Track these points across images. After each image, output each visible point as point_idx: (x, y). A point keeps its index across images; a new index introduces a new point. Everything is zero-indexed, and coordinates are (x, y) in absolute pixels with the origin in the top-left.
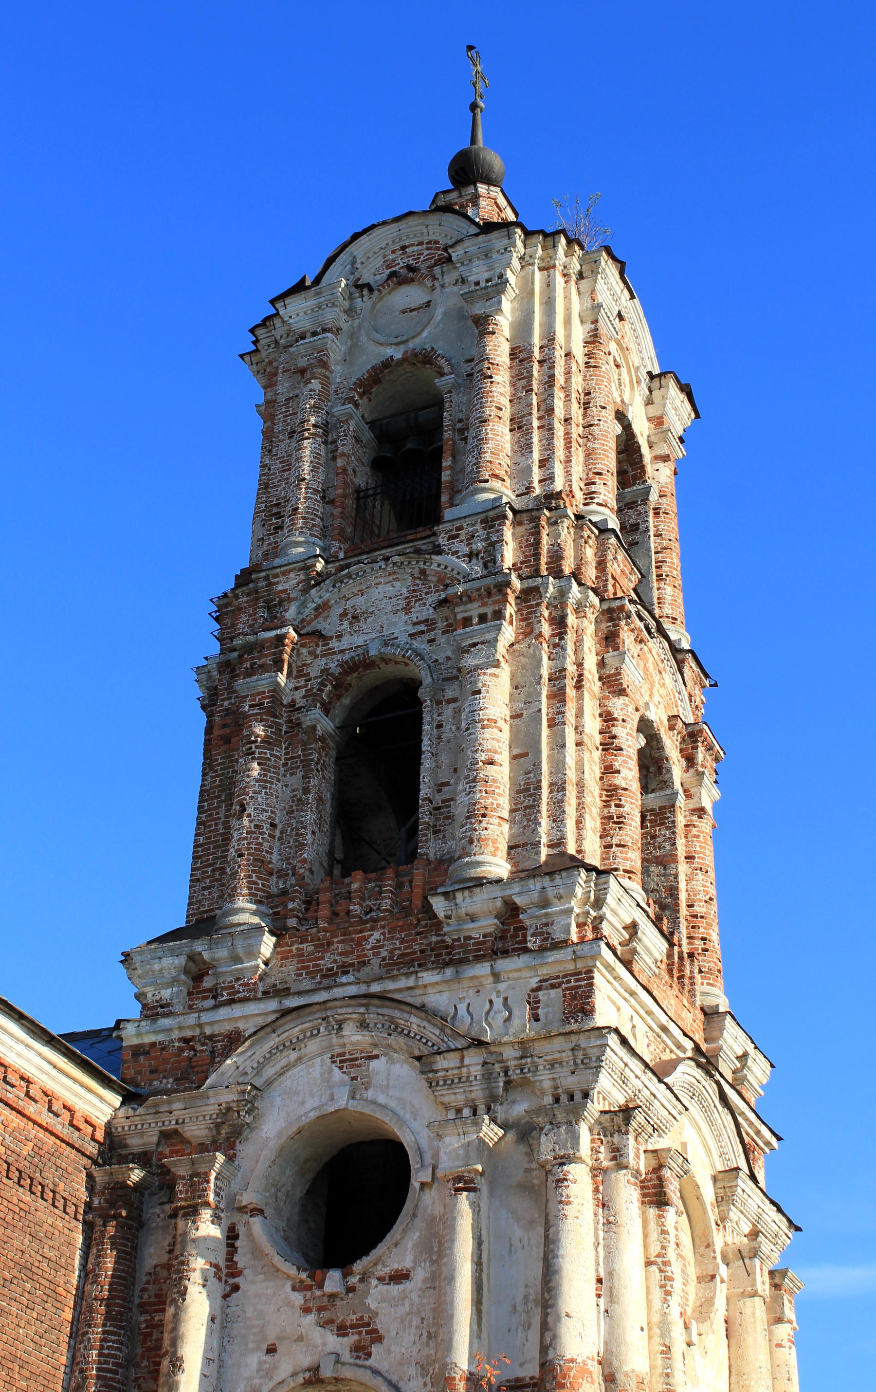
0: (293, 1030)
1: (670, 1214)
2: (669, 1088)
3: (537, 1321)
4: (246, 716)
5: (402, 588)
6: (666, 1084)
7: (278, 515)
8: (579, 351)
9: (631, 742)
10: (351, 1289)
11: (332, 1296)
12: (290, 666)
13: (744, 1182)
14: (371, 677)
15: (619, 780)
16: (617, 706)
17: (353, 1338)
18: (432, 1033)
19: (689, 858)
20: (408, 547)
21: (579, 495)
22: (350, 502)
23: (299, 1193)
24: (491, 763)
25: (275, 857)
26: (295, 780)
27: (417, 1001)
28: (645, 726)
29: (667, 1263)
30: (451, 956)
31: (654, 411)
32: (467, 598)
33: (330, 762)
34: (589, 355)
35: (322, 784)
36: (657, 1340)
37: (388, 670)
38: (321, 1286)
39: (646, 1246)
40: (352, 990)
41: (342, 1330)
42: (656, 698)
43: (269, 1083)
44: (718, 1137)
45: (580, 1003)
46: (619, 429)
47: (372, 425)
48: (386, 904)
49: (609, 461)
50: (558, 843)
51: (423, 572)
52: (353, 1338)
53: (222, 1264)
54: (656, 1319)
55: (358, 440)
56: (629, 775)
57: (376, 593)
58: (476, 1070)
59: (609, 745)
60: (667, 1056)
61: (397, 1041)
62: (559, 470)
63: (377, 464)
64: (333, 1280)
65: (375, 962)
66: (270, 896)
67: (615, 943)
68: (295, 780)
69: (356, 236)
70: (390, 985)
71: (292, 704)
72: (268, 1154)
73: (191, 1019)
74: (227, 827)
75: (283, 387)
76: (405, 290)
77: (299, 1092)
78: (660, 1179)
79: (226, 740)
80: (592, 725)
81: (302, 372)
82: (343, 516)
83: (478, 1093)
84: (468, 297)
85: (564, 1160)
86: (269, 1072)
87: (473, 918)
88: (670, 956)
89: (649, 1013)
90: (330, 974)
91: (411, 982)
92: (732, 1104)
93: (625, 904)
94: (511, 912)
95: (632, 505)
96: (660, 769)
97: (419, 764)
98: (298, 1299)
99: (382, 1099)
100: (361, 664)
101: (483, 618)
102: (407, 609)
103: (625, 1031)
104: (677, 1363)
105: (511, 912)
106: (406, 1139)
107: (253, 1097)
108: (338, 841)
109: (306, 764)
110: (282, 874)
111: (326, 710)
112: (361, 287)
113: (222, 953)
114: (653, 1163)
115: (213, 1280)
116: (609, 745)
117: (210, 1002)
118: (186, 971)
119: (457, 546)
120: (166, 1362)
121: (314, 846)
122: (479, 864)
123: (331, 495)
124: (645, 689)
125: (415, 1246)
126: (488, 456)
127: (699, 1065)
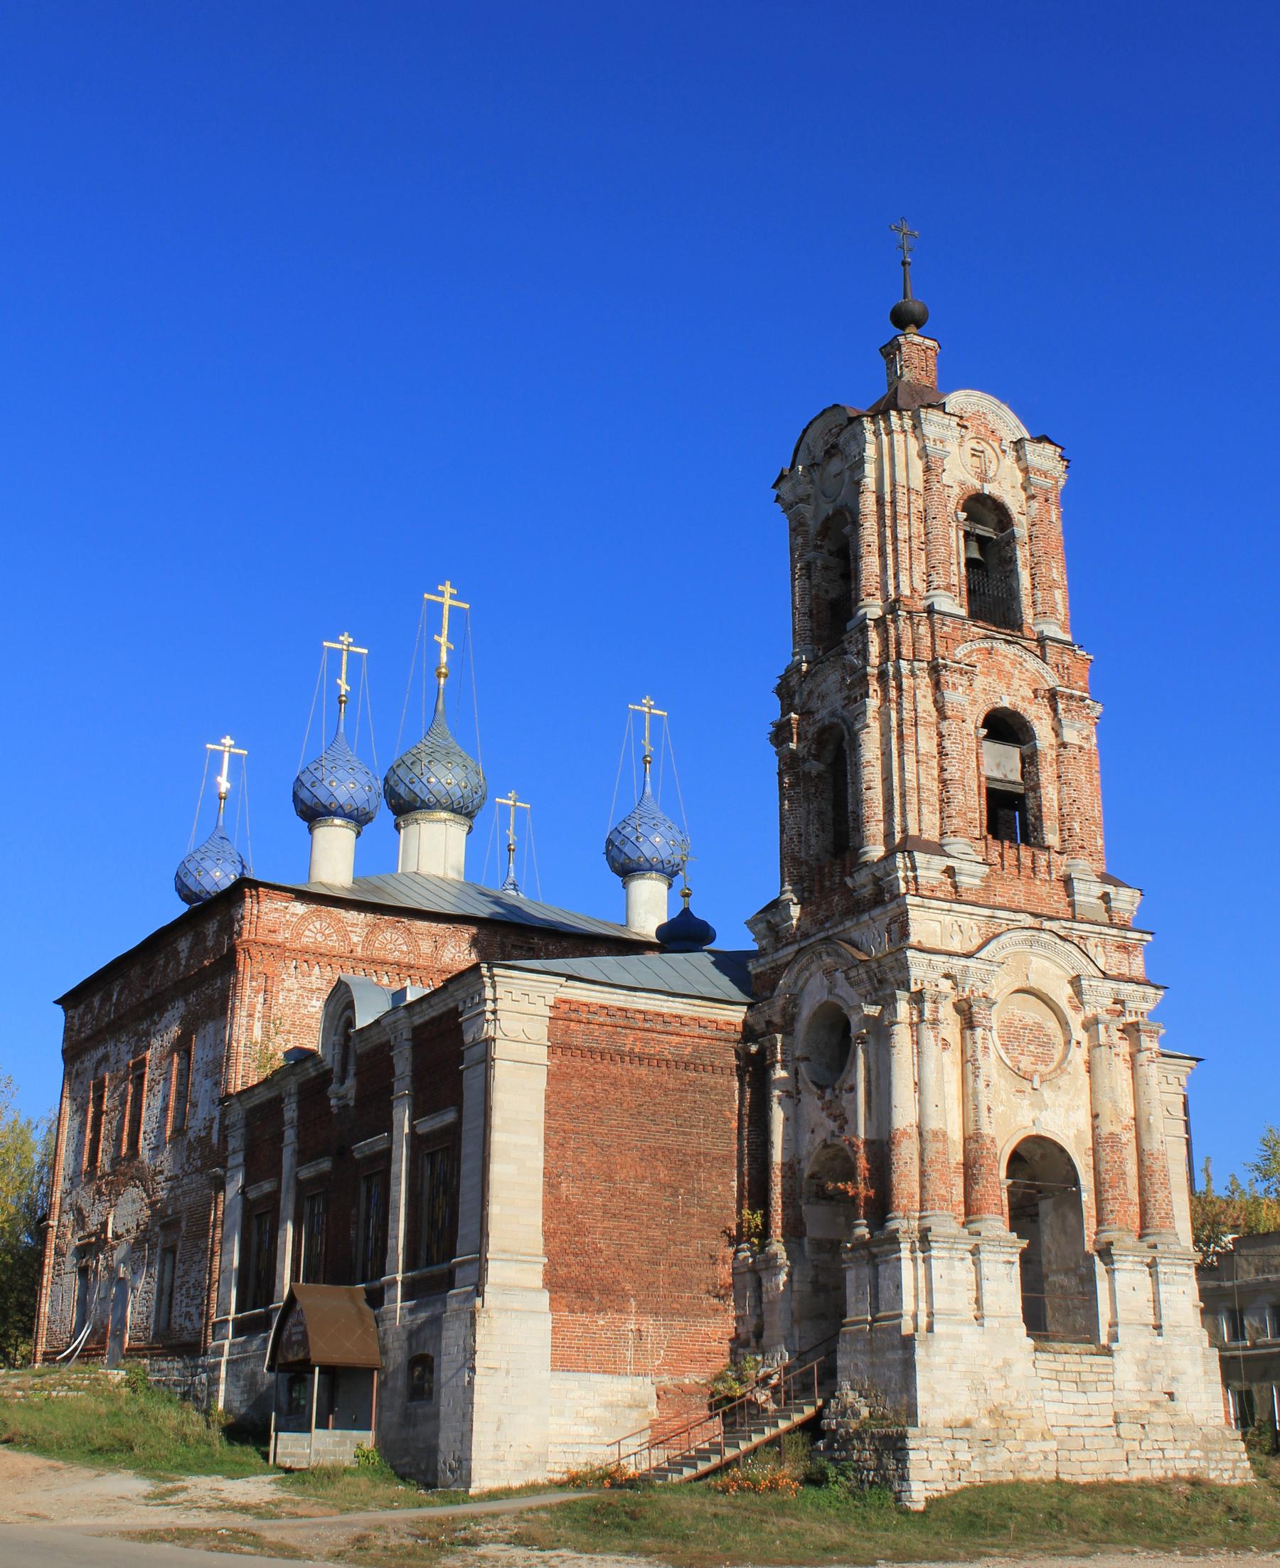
12: (798, 734)
24: (869, 788)
25: (803, 854)
43: (802, 989)
50: (904, 830)
58: (864, 976)
69: (805, 431)
85: (893, 1024)
86: (800, 983)
92: (391, 1198)
107: (794, 1000)
115: (784, 1099)
122: (865, 853)
126: (863, 583)
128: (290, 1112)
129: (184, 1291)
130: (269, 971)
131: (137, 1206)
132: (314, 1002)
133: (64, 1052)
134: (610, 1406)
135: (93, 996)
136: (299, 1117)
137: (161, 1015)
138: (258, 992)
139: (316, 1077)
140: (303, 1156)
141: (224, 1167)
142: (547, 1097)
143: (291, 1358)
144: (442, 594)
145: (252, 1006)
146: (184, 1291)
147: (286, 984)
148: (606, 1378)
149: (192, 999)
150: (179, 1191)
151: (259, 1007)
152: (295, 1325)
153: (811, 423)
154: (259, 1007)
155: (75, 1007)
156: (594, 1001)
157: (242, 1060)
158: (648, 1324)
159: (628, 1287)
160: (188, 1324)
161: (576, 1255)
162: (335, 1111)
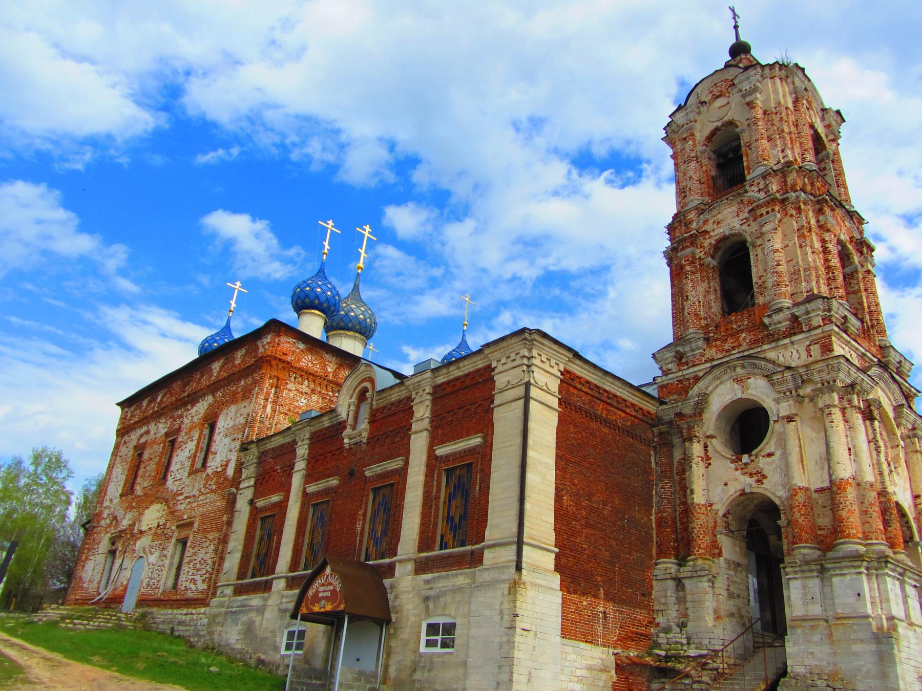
0: (717, 372)
1: (876, 423)
2: (869, 376)
3: (826, 466)
4: (684, 265)
5: (735, 208)
6: (869, 376)
7: (684, 192)
8: (790, 106)
9: (833, 248)
10: (752, 461)
11: (746, 464)
13: (906, 410)
14: (728, 243)
15: (832, 264)
16: (827, 236)
17: (755, 478)
18: (770, 366)
19: (866, 290)
20: (735, 193)
21: (799, 160)
22: (711, 182)
23: (728, 429)
25: (702, 313)
26: (705, 285)
27: (763, 356)
28: (839, 242)
29: (877, 441)
30: (773, 337)
31: (826, 123)
32: (761, 206)
33: (717, 275)
34: (795, 106)
35: (716, 284)
36: (876, 470)
37: (734, 239)
38: (741, 460)
39: (867, 435)
40: (738, 355)
41: (751, 475)
42: (843, 231)
44: (893, 394)
45: (827, 348)
46: (812, 132)
47: (714, 152)
48: (746, 323)
49: (810, 144)
51: (742, 201)
52: (755, 478)
53: (703, 455)
54: (875, 462)
55: (710, 159)
56: (835, 261)
57: (725, 212)
58: (789, 378)
59: (825, 251)
60: (867, 365)
61: (756, 371)
62: (789, 152)
63: (719, 166)
64: (745, 458)
65: (745, 344)
66: (702, 327)
67: (839, 324)
68: (705, 285)
70: (752, 352)
71: (700, 258)
72: (714, 417)
73: (680, 373)
74: (683, 305)
75: (679, 146)
76: (719, 100)
77: (722, 395)
78: (871, 410)
79: (678, 275)
80: (817, 245)
81: (685, 139)
82: (708, 187)
83: (791, 386)
84: (744, 96)
86: (710, 388)
87: (780, 323)
88: (863, 327)
89: (857, 349)
90: (728, 351)
91: (759, 349)
93: (840, 308)
94: (795, 319)
95: (822, 161)
96: (849, 258)
97: (751, 271)
98: (733, 466)
99: (754, 393)
100: (724, 239)
101: (767, 213)
102: (738, 216)
103: (848, 356)
104: (887, 478)
105: (795, 319)
106: (765, 406)
108: (725, 305)
109: (708, 278)
110: (705, 319)
111: (713, 257)
112: (703, 103)
113: (687, 349)
114: (866, 404)
116: (825, 251)
117: (686, 367)
118: (675, 357)
119: (753, 188)
120: (688, 491)
121: (716, 307)
123: (703, 180)
124: (838, 228)
125: (775, 443)
127: (881, 366)
128: (302, 451)
129: (191, 566)
130: (281, 376)
131: (160, 514)
132: (302, 400)
133: (118, 431)
134: (590, 668)
135: (143, 400)
136: (309, 454)
137: (193, 405)
138: (272, 387)
139: (328, 428)
140: (310, 477)
141: (237, 488)
142: (557, 433)
143: (316, 609)
144: (365, 230)
145: (268, 394)
146: (191, 566)
147: (288, 386)
148: (588, 646)
149: (219, 394)
150: (195, 504)
151: (272, 396)
152: (323, 585)
153: (703, 80)
154: (272, 396)
155: (129, 407)
156: (583, 376)
157: (258, 424)
158: (610, 608)
159: (599, 579)
160: (192, 586)
161: (571, 551)
162: (347, 446)
